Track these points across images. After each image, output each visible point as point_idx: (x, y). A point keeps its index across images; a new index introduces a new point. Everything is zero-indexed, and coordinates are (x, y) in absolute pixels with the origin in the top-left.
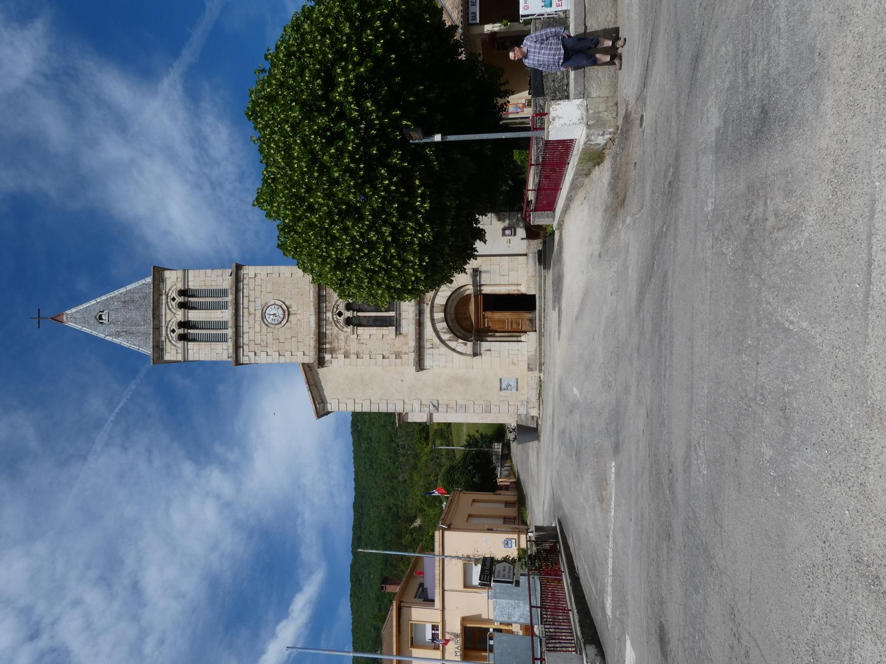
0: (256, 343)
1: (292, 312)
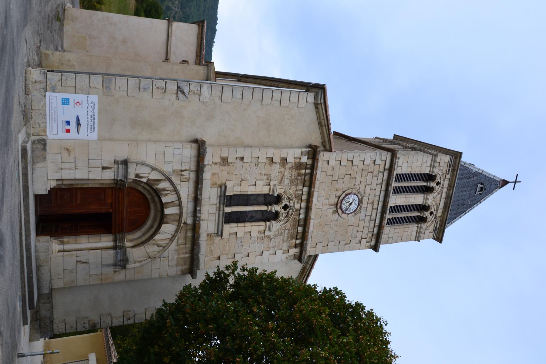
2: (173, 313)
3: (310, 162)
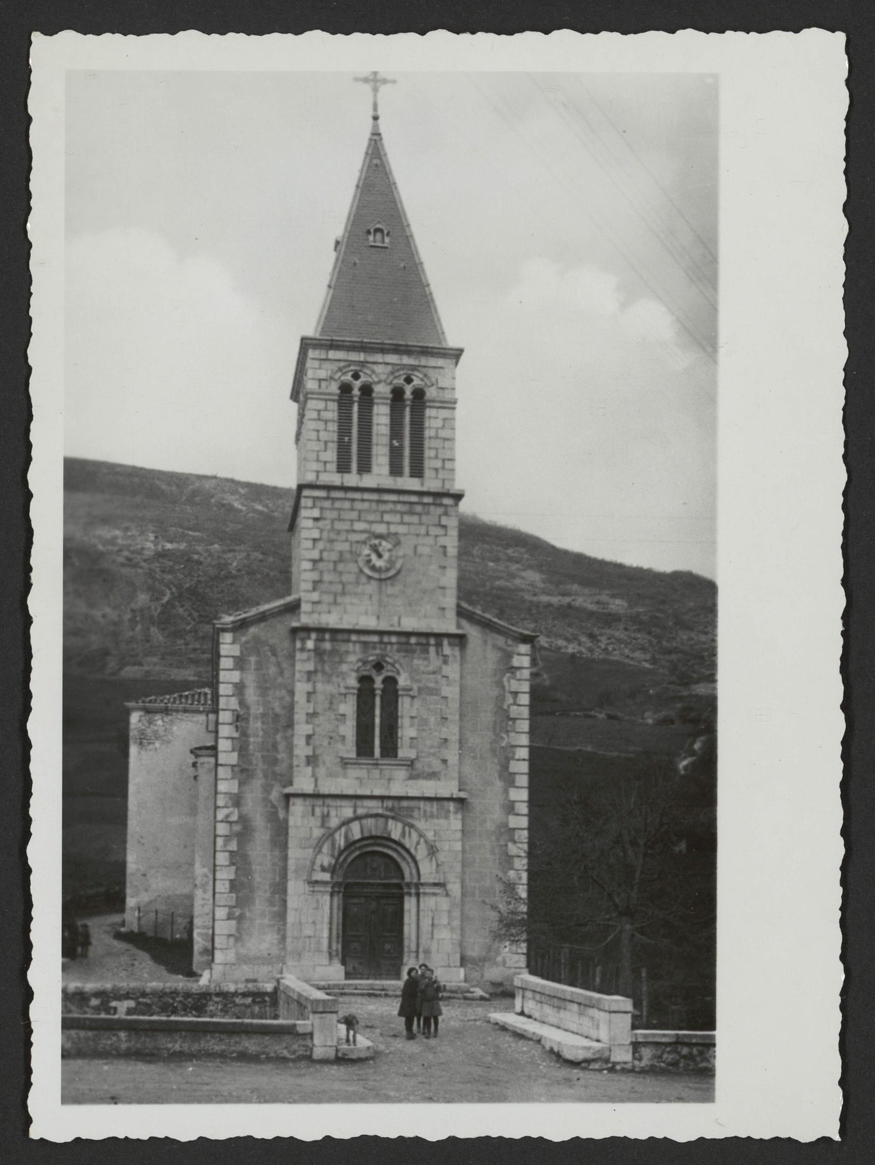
0: (357, 518)
1: (384, 587)
2: (204, 1002)
3: (314, 636)
